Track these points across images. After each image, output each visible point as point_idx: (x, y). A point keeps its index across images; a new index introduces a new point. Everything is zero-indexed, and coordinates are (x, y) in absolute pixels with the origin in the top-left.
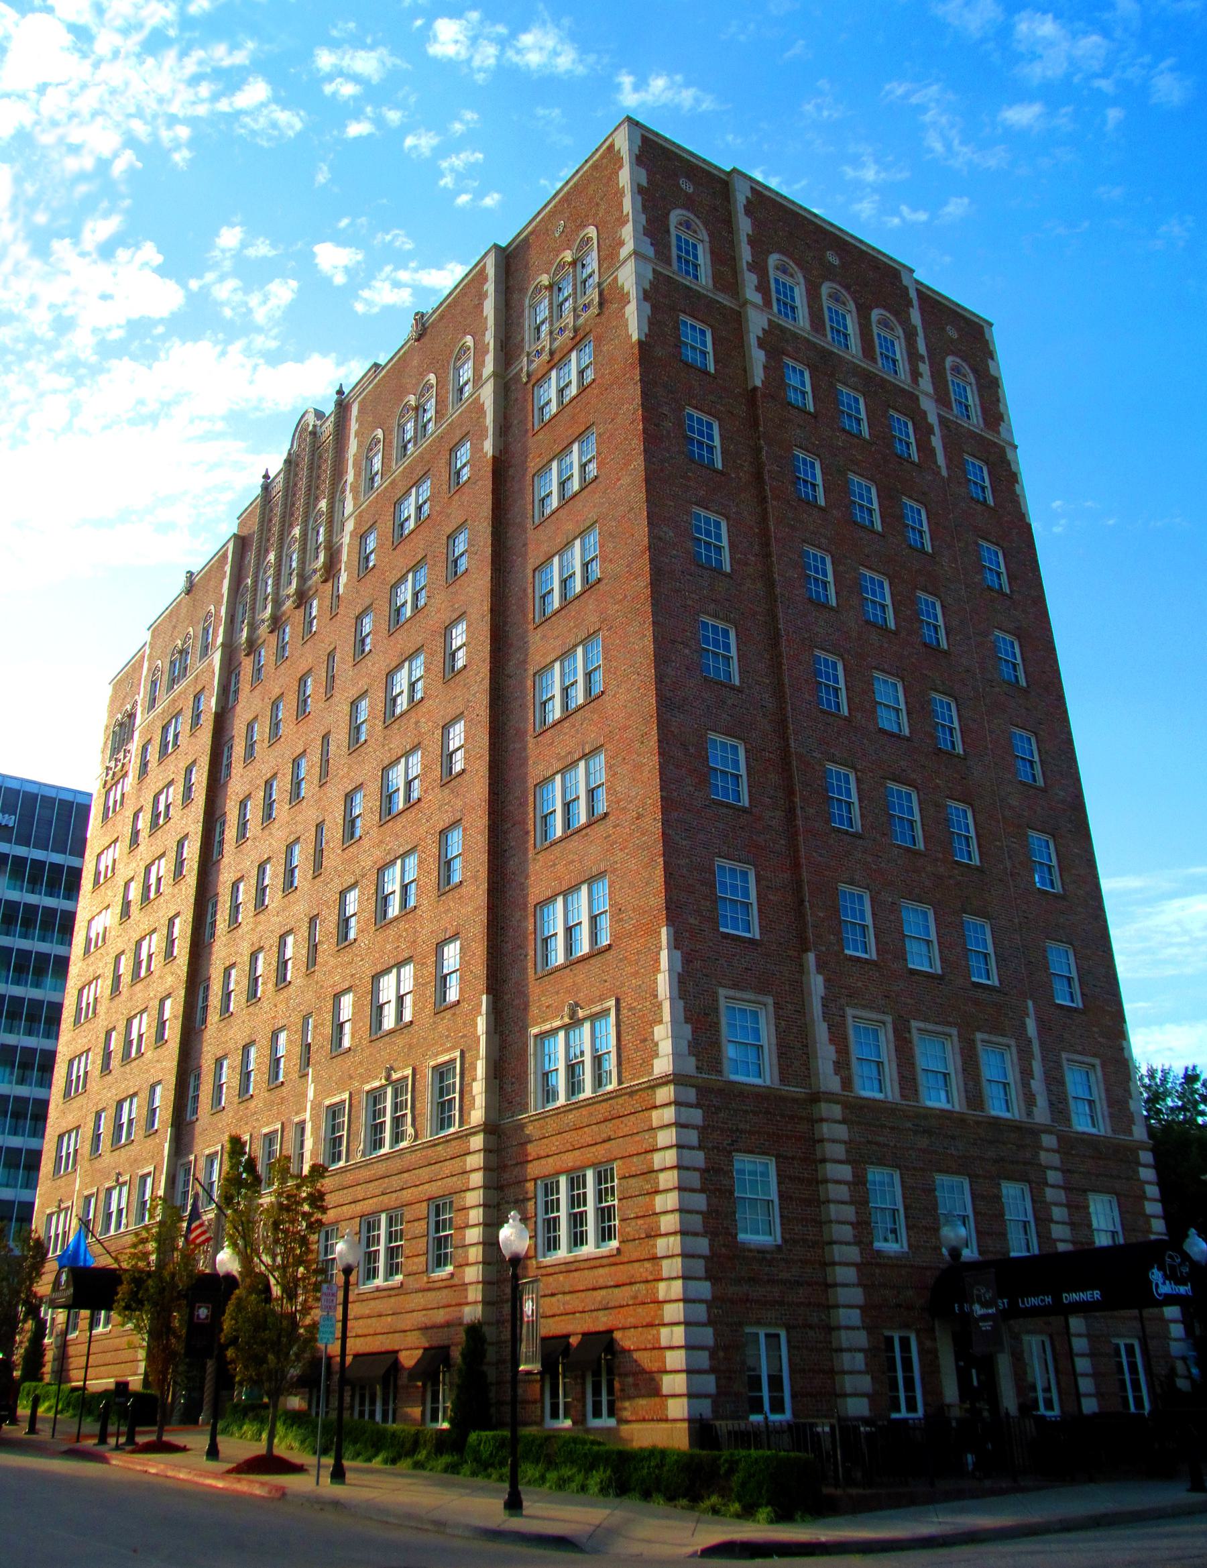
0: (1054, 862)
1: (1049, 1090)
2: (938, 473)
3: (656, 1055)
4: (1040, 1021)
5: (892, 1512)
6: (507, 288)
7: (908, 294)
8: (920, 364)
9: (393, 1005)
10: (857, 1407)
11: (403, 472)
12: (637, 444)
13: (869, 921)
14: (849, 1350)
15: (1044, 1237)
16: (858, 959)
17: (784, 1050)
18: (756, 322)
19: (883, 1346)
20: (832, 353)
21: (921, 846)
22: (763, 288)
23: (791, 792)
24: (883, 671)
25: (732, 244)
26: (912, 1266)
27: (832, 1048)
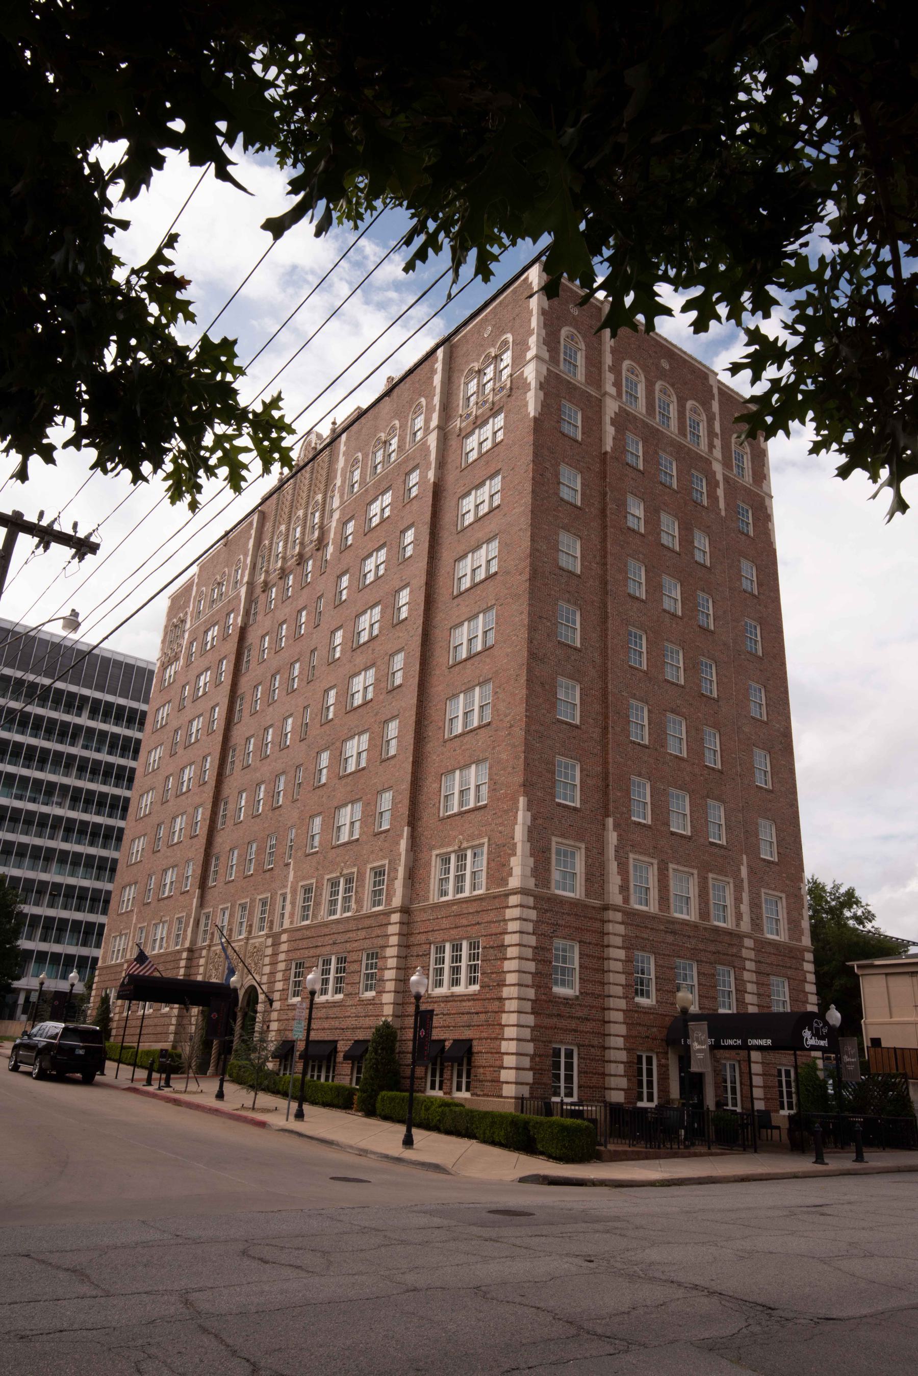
0: (769, 769)
1: (751, 911)
2: (719, 514)
3: (511, 875)
4: (749, 866)
6: (450, 368)
7: (712, 391)
8: (715, 440)
9: (348, 826)
10: (617, 1097)
11: (373, 484)
12: (528, 487)
13: (648, 800)
14: (615, 1062)
15: (741, 1002)
16: (639, 823)
17: (590, 878)
18: (611, 407)
19: (636, 1061)
20: (658, 430)
21: (685, 755)
22: (617, 384)
23: (606, 717)
24: (671, 642)
25: (600, 352)
26: (657, 1014)
27: (619, 877)
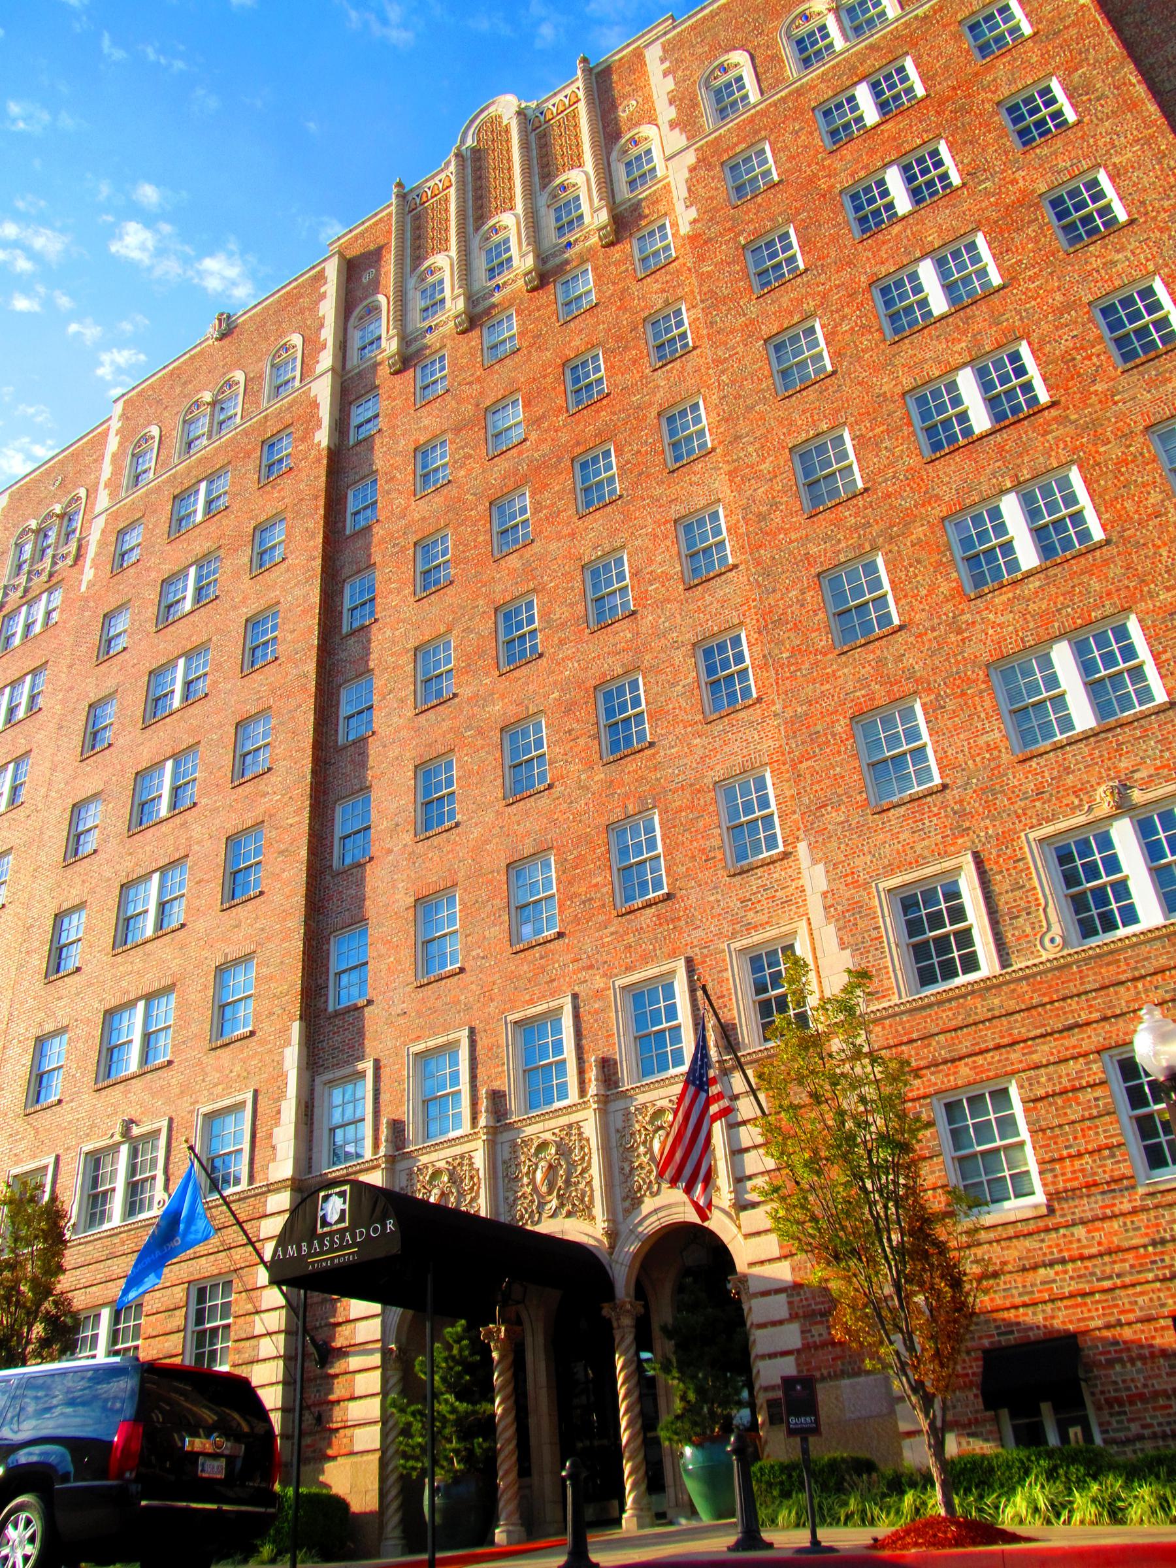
5: (700, 1558)
